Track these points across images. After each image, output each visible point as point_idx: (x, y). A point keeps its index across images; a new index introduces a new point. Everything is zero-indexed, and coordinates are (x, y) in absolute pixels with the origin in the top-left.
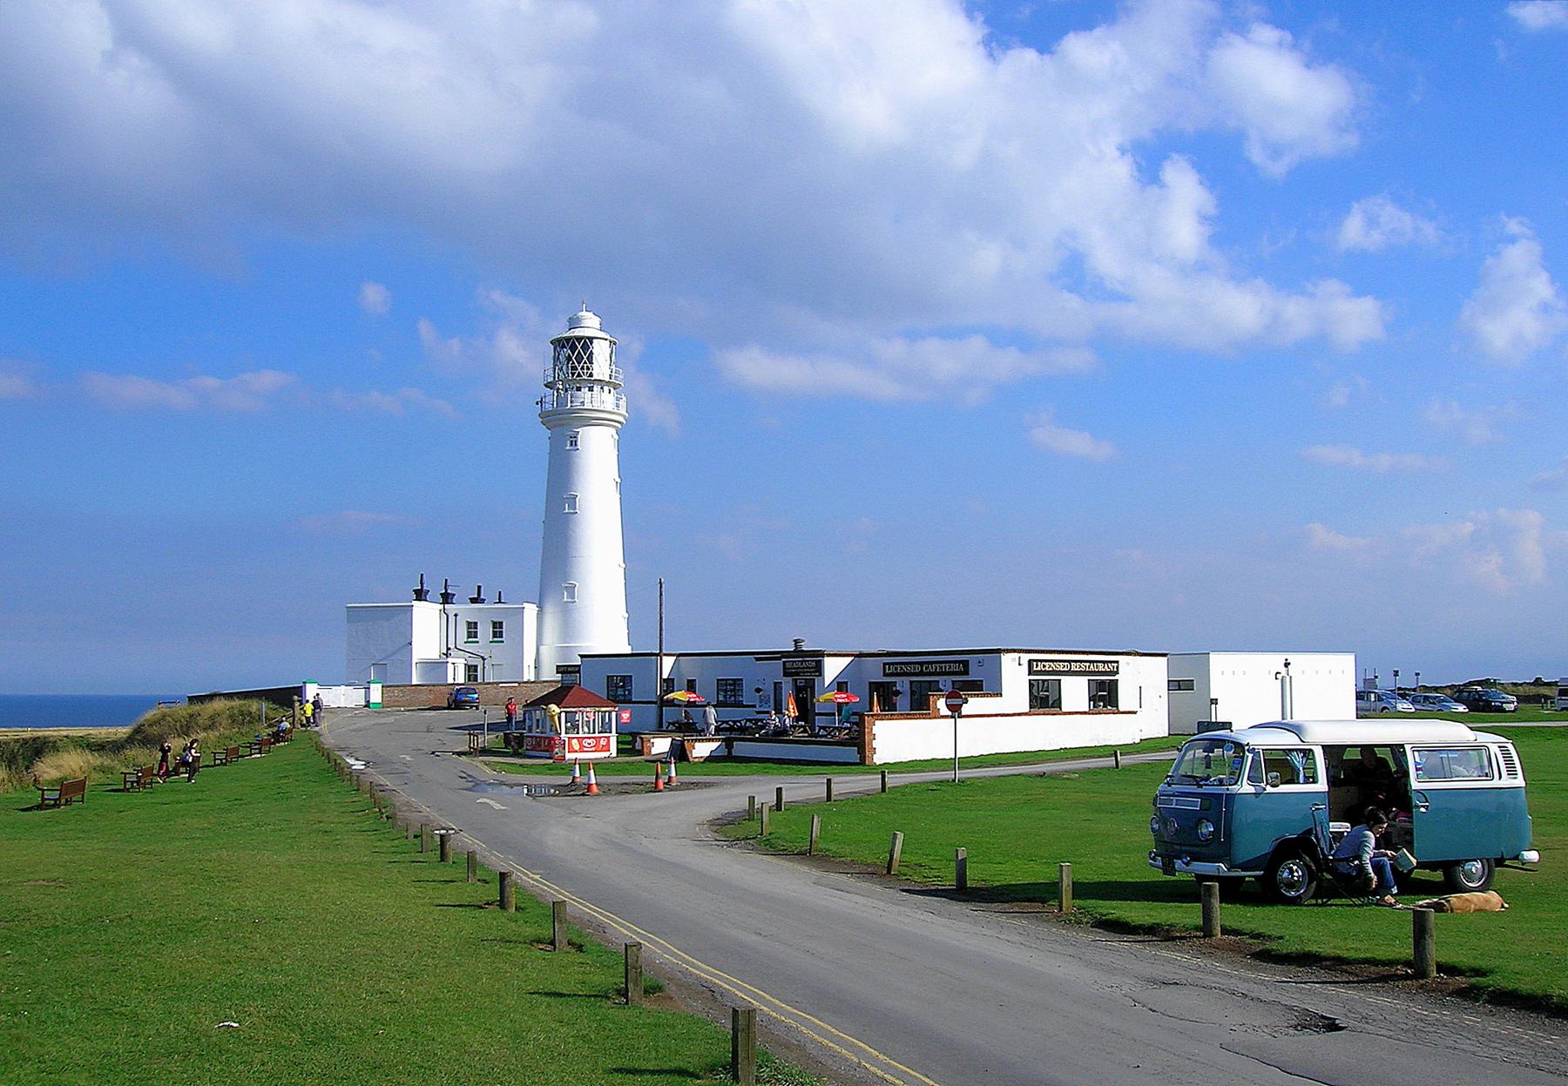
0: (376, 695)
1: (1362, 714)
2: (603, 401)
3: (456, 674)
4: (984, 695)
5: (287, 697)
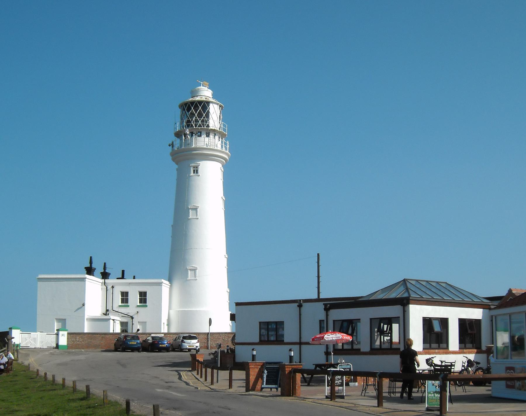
0: (63, 341)
1: (334, 321)
3: (115, 327)
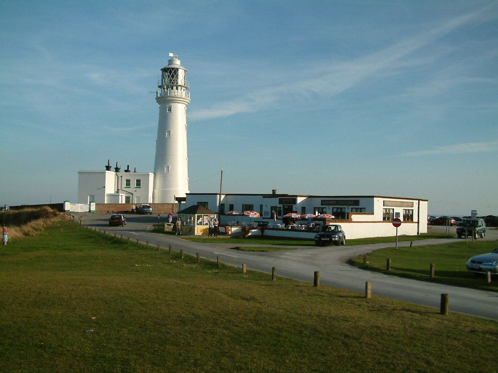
0: (93, 208)
2: (181, 93)
4: (362, 214)
5: (60, 207)
